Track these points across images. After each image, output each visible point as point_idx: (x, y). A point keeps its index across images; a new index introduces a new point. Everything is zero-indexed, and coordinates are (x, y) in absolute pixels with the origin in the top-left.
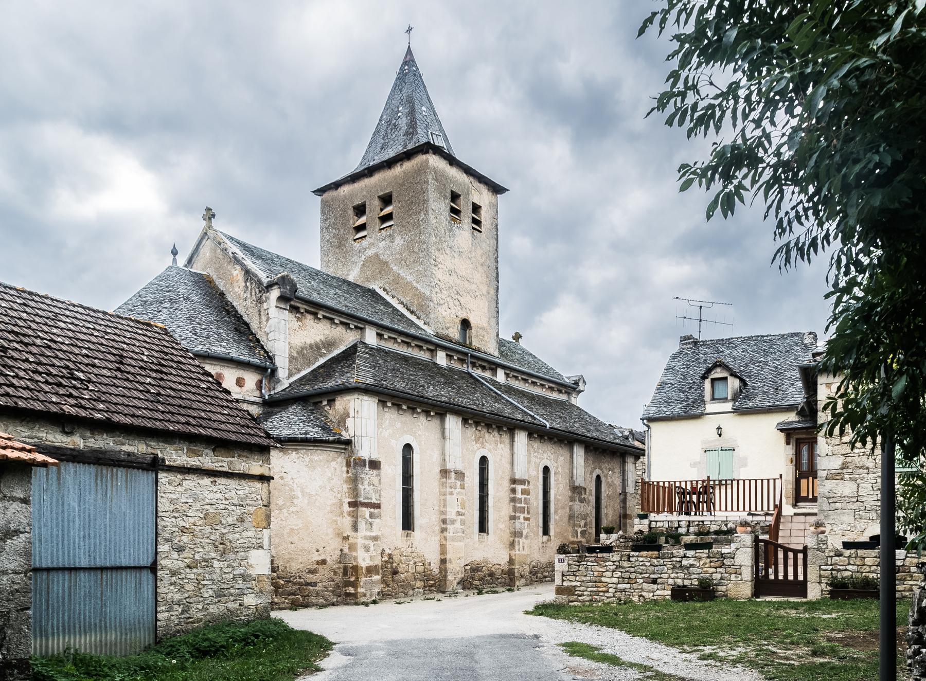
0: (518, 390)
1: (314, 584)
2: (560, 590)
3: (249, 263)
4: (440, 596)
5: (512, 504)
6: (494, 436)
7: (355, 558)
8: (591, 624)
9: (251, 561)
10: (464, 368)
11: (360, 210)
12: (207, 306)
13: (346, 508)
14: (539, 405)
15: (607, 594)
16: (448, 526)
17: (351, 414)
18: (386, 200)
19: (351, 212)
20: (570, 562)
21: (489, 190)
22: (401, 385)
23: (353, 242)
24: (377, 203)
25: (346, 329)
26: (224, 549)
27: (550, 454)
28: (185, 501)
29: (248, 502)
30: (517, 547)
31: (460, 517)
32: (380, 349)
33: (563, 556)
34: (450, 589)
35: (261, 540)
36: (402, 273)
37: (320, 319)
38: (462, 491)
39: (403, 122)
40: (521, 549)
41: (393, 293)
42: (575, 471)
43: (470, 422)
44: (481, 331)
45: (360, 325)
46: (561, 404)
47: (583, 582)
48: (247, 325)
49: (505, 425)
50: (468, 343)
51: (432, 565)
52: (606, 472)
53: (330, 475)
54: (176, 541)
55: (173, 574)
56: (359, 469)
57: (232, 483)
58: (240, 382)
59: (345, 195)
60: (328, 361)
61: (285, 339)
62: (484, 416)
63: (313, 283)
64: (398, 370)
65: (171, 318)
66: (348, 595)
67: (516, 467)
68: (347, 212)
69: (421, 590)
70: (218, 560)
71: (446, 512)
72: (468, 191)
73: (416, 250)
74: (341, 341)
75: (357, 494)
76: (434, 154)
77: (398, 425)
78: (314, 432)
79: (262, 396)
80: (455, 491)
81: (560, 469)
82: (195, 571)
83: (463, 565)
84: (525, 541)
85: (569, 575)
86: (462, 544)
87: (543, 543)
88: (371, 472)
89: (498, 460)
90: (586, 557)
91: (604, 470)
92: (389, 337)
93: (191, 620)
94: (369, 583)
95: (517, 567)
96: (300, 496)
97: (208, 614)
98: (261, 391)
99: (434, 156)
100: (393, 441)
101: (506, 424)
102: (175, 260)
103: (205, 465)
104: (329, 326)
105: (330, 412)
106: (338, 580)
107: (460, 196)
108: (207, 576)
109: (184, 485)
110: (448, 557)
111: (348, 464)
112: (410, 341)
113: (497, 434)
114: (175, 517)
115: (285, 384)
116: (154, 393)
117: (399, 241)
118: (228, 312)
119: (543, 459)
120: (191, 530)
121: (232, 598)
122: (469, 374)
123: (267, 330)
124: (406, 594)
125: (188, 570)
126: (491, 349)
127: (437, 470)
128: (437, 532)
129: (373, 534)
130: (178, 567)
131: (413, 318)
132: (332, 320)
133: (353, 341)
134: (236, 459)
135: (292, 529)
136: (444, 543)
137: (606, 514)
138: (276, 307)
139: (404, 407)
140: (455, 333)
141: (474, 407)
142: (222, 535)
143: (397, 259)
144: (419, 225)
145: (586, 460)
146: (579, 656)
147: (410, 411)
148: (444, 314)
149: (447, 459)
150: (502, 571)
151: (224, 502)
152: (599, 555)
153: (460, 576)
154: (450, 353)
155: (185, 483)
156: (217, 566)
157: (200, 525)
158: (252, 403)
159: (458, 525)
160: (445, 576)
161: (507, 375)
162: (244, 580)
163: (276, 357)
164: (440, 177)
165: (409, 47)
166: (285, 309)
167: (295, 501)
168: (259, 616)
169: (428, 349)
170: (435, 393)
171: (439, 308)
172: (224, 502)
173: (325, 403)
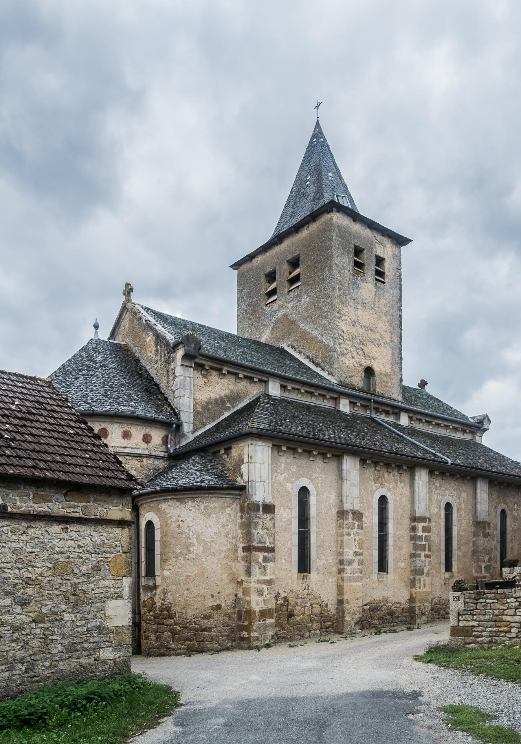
0: (421, 432)
1: (209, 629)
2: (455, 631)
3: (160, 328)
4: (335, 638)
5: (412, 542)
6: (393, 476)
7: (249, 603)
8: (487, 676)
9: (109, 612)
10: (368, 414)
11: (271, 277)
12: (121, 371)
13: (241, 553)
14: (443, 444)
15: (509, 635)
16: (346, 567)
17: (246, 460)
18: (294, 263)
19: (263, 280)
20: (466, 600)
21: (392, 242)
22: (297, 429)
23: (265, 307)
24: (286, 267)
26: (77, 600)
27: (452, 491)
28: (30, 550)
29: (105, 549)
30: (417, 585)
31: (358, 557)
32: (283, 399)
33: (458, 594)
34: (348, 630)
35: (120, 590)
36: (308, 329)
37: (225, 374)
38: (360, 531)
39: (311, 190)
40: (422, 587)
41: (300, 349)
42: (478, 506)
43: (368, 462)
44: (384, 378)
45: (264, 378)
46: (466, 443)
47: (481, 621)
48: (157, 385)
49: (405, 464)
50: (372, 390)
51: (329, 606)
52: (511, 506)
53: (225, 521)
54: (19, 594)
55: (15, 629)
56: (253, 514)
57: (87, 530)
58: (147, 439)
59: (258, 265)
60: (232, 414)
61: (190, 395)
62: (382, 456)
63: (221, 343)
64: (298, 417)
65: (86, 383)
66: (242, 639)
67: (416, 505)
68: (260, 281)
69: (318, 632)
70: (70, 613)
71: (343, 552)
73: (321, 305)
74: (245, 394)
75: (250, 538)
76: (338, 212)
77: (294, 469)
78: (209, 480)
79: (168, 450)
80: (352, 532)
81: (463, 506)
82: (41, 625)
83: (361, 604)
84: (426, 578)
85: (466, 614)
86: (359, 584)
87: (445, 579)
88: (265, 517)
89: (398, 499)
90: (485, 593)
91: (509, 504)
92: (293, 388)
93: (36, 679)
94: (262, 626)
95: (418, 604)
96: (196, 543)
97: (57, 672)
98: (167, 446)
99: (338, 214)
101: (330, 448)
102: (96, 333)
103: (55, 511)
104: (234, 381)
105: (228, 460)
106: (233, 625)
107: (363, 250)
108: (56, 630)
109: (30, 533)
110: (346, 597)
111: (242, 510)
112: (299, 387)
113: (396, 473)
114: (18, 568)
115: (191, 438)
116: (8, 438)
117: (306, 299)
118: (141, 376)
119: (445, 496)
120: (36, 582)
121: (86, 653)
123: (173, 388)
124: (302, 637)
125: (33, 625)
126: (396, 395)
127: (334, 511)
128: (335, 573)
129: (267, 578)
130: (21, 622)
131: (318, 370)
132: (236, 374)
134: (91, 503)
135: (188, 576)
136: (341, 584)
137: (512, 548)
138: (182, 365)
139: (300, 451)
140: (358, 381)
141: (373, 447)
142: (75, 586)
143: (304, 317)
145: (490, 495)
146: (463, 731)
147: (307, 454)
148: (348, 363)
149: (345, 500)
150: (403, 609)
151: (77, 550)
152: (499, 591)
153: (358, 616)
154: (353, 400)
155: (31, 531)
156: (68, 619)
157: (49, 576)
158: (158, 458)
159: (355, 565)
160: (343, 617)
161: (411, 418)
162: (101, 633)
163: (181, 413)
164: (343, 233)
165: (318, 121)
166: (190, 367)
167: (191, 548)
168: (118, 671)
169: (331, 398)
170: (333, 436)
171: (343, 358)
172: (77, 550)
173: (222, 452)
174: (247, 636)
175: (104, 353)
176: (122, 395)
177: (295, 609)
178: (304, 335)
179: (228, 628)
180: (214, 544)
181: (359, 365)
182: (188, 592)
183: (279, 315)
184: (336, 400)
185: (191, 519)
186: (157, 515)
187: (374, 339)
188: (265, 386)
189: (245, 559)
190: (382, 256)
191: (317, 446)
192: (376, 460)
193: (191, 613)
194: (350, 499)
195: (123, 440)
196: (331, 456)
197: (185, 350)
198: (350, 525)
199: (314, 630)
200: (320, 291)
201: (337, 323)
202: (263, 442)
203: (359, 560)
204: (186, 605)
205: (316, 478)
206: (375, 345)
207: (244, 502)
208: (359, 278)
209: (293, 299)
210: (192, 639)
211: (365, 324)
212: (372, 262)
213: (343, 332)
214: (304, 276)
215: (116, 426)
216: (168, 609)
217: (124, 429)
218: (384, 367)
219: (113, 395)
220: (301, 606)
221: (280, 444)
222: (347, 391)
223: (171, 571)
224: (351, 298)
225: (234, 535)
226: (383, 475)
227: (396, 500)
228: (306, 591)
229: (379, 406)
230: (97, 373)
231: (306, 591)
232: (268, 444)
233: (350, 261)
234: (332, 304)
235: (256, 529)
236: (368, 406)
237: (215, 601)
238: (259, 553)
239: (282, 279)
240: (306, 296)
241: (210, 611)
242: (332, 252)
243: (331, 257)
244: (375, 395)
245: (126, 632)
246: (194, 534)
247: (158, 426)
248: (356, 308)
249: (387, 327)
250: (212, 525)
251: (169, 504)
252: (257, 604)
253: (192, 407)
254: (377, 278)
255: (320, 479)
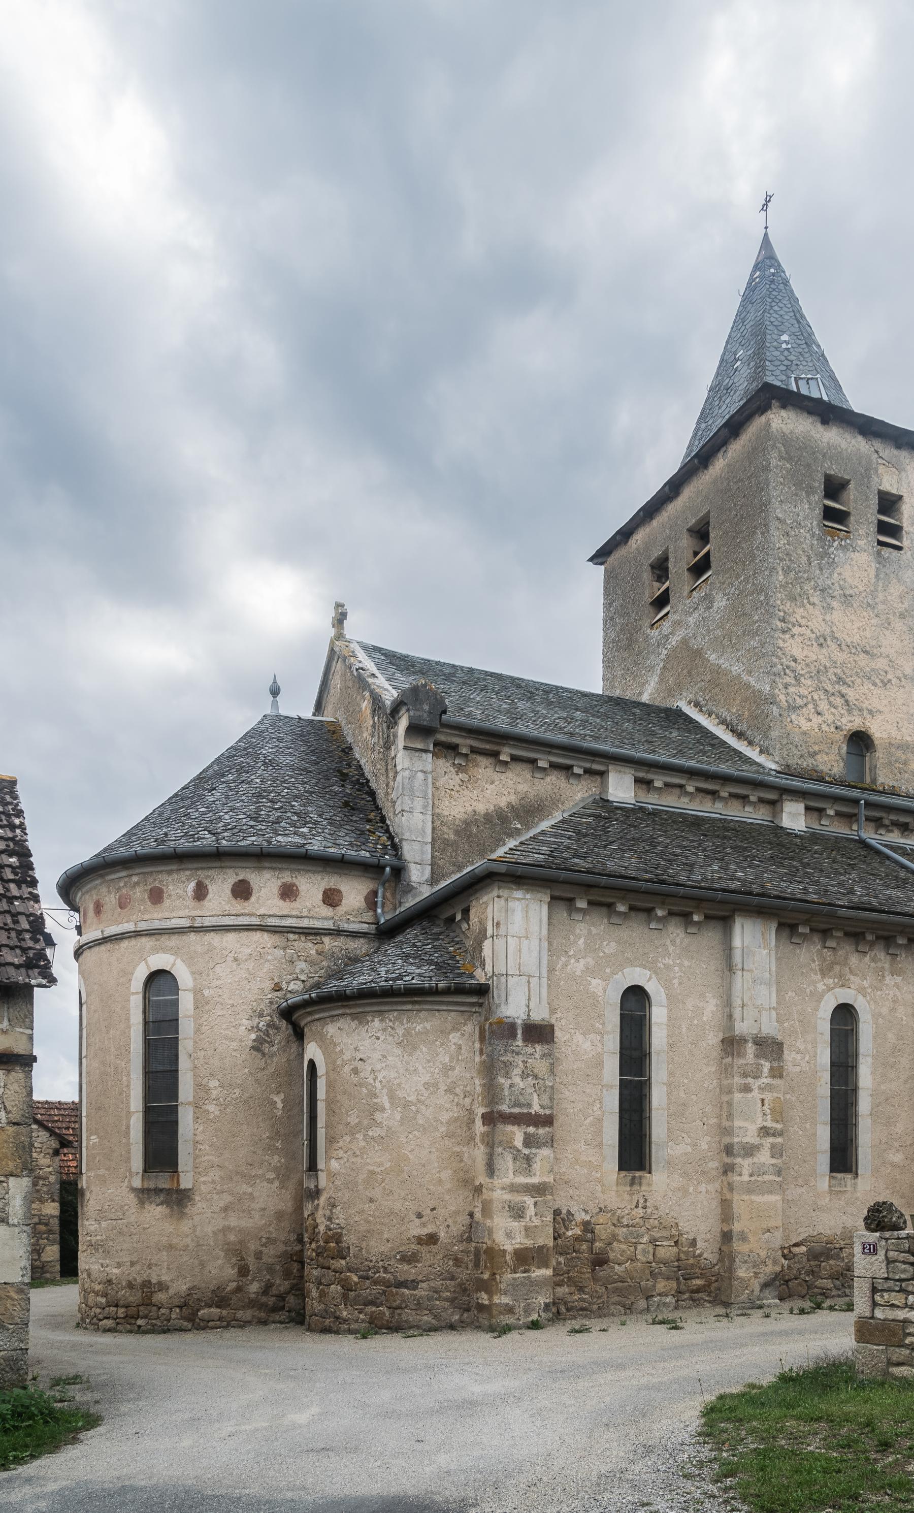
1: (413, 1284)
6: (873, 960)
13: (479, 1128)
16: (738, 1160)
17: (489, 932)
19: (647, 576)
20: (891, 1254)
25: (568, 778)
31: (771, 1140)
37: (506, 763)
38: (777, 1081)
44: (899, 753)
45: (596, 767)
48: (372, 794)
53: (447, 1060)
56: (499, 1045)
58: (331, 898)
59: (638, 549)
61: (425, 807)
62: (833, 915)
66: (481, 1308)
71: (732, 1128)
72: (867, 470)
73: (748, 608)
74: (555, 802)
76: (784, 407)
85: (889, 1290)
86: (774, 1198)
88: (530, 1050)
89: (885, 1011)
94: (523, 1284)
96: (387, 1105)
98: (375, 911)
99: (783, 413)
100: (595, 982)
101: (698, 901)
102: (275, 704)
104: (529, 776)
110: (737, 1227)
112: (683, 782)
113: (882, 955)
117: (720, 602)
118: (344, 777)
122: (863, 844)
127: (713, 1039)
129: (534, 1180)
132: (568, 768)
133: (583, 799)
135: (372, 1173)
136: (728, 1197)
138: (406, 748)
139: (621, 908)
144: (753, 557)
148: (805, 726)
149: (737, 1013)
153: (770, 1269)
158: (354, 935)
159: (764, 1157)
160: (731, 1270)
163: (404, 843)
165: (766, 235)
166: (426, 751)
167: (378, 1116)
169: (761, 801)
171: (793, 717)
174: (487, 1302)
175: (280, 740)
176: (289, 814)
177: (612, 1249)
178: (717, 675)
179: (453, 1283)
180: (423, 1107)
181: (833, 729)
182: (373, 1205)
183: (674, 643)
184: (774, 805)
185: (377, 1056)
186: (320, 1047)
187: (873, 670)
188: (602, 783)
189: (486, 1139)
190: (894, 491)
191: (664, 897)
192: (886, 934)
193: (376, 1248)
194: (750, 1013)
195: (282, 902)
196: (702, 918)
197: (410, 716)
198: (749, 1068)
199: (660, 1295)
200: (746, 581)
201: (780, 642)
202: (527, 891)
203: (773, 1146)
204: (369, 1231)
205: (668, 967)
206: (875, 684)
207: (486, 1019)
208: (836, 543)
209: (698, 605)
210: (378, 1301)
211: (849, 640)
212: (868, 506)
213: (795, 661)
214: (717, 555)
215: (267, 875)
216: (337, 1238)
217: (284, 880)
218: (899, 729)
219: (269, 816)
220: (627, 1242)
221: (572, 896)
222: (797, 783)
223: (342, 1161)
224: (815, 588)
225: (468, 1089)
226: (846, 959)
227: (880, 1014)
228: (640, 1212)
229: (883, 815)
230: (252, 777)
231: (640, 1212)
232: (539, 896)
233: (812, 510)
234: (767, 604)
235: (507, 1076)
236: (855, 815)
237: (424, 1225)
238: (515, 1128)
239: (679, 568)
240: (721, 595)
241: (414, 1247)
242: (769, 495)
243: (766, 506)
244: (874, 790)
245: (15, 1296)
246: (383, 1087)
247: (356, 873)
248: (830, 608)
249: (906, 643)
250: (420, 1068)
251: (339, 1025)
252: (509, 1235)
253: (429, 831)
254: (883, 539)
255: (677, 969)
